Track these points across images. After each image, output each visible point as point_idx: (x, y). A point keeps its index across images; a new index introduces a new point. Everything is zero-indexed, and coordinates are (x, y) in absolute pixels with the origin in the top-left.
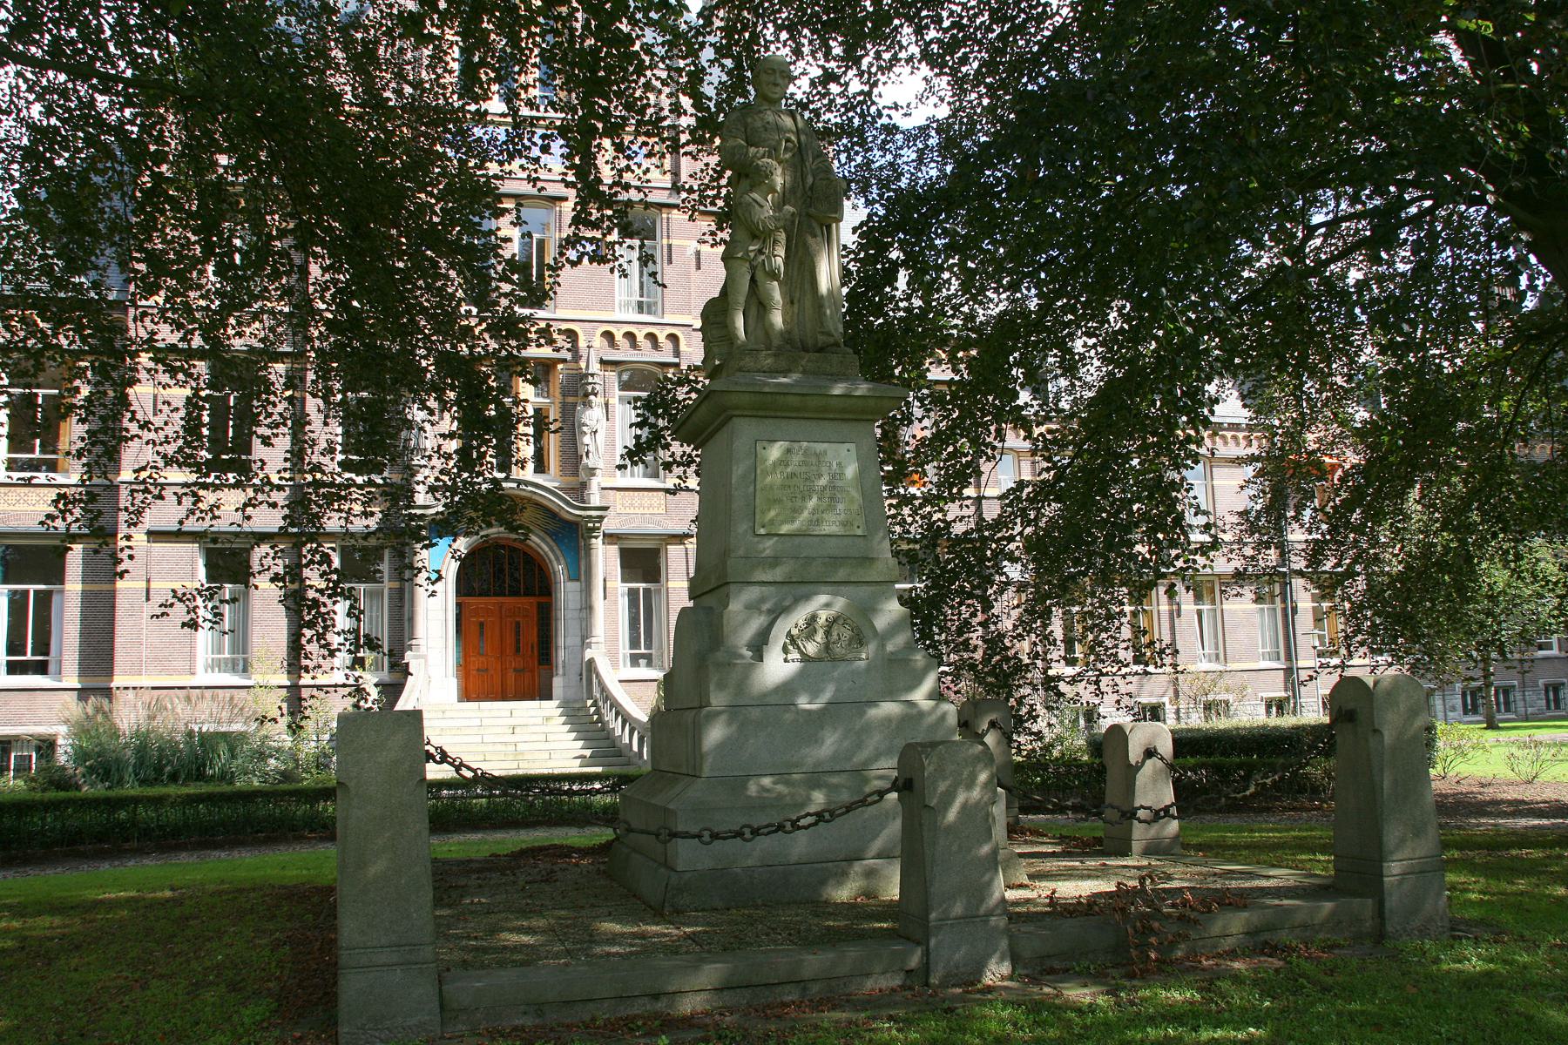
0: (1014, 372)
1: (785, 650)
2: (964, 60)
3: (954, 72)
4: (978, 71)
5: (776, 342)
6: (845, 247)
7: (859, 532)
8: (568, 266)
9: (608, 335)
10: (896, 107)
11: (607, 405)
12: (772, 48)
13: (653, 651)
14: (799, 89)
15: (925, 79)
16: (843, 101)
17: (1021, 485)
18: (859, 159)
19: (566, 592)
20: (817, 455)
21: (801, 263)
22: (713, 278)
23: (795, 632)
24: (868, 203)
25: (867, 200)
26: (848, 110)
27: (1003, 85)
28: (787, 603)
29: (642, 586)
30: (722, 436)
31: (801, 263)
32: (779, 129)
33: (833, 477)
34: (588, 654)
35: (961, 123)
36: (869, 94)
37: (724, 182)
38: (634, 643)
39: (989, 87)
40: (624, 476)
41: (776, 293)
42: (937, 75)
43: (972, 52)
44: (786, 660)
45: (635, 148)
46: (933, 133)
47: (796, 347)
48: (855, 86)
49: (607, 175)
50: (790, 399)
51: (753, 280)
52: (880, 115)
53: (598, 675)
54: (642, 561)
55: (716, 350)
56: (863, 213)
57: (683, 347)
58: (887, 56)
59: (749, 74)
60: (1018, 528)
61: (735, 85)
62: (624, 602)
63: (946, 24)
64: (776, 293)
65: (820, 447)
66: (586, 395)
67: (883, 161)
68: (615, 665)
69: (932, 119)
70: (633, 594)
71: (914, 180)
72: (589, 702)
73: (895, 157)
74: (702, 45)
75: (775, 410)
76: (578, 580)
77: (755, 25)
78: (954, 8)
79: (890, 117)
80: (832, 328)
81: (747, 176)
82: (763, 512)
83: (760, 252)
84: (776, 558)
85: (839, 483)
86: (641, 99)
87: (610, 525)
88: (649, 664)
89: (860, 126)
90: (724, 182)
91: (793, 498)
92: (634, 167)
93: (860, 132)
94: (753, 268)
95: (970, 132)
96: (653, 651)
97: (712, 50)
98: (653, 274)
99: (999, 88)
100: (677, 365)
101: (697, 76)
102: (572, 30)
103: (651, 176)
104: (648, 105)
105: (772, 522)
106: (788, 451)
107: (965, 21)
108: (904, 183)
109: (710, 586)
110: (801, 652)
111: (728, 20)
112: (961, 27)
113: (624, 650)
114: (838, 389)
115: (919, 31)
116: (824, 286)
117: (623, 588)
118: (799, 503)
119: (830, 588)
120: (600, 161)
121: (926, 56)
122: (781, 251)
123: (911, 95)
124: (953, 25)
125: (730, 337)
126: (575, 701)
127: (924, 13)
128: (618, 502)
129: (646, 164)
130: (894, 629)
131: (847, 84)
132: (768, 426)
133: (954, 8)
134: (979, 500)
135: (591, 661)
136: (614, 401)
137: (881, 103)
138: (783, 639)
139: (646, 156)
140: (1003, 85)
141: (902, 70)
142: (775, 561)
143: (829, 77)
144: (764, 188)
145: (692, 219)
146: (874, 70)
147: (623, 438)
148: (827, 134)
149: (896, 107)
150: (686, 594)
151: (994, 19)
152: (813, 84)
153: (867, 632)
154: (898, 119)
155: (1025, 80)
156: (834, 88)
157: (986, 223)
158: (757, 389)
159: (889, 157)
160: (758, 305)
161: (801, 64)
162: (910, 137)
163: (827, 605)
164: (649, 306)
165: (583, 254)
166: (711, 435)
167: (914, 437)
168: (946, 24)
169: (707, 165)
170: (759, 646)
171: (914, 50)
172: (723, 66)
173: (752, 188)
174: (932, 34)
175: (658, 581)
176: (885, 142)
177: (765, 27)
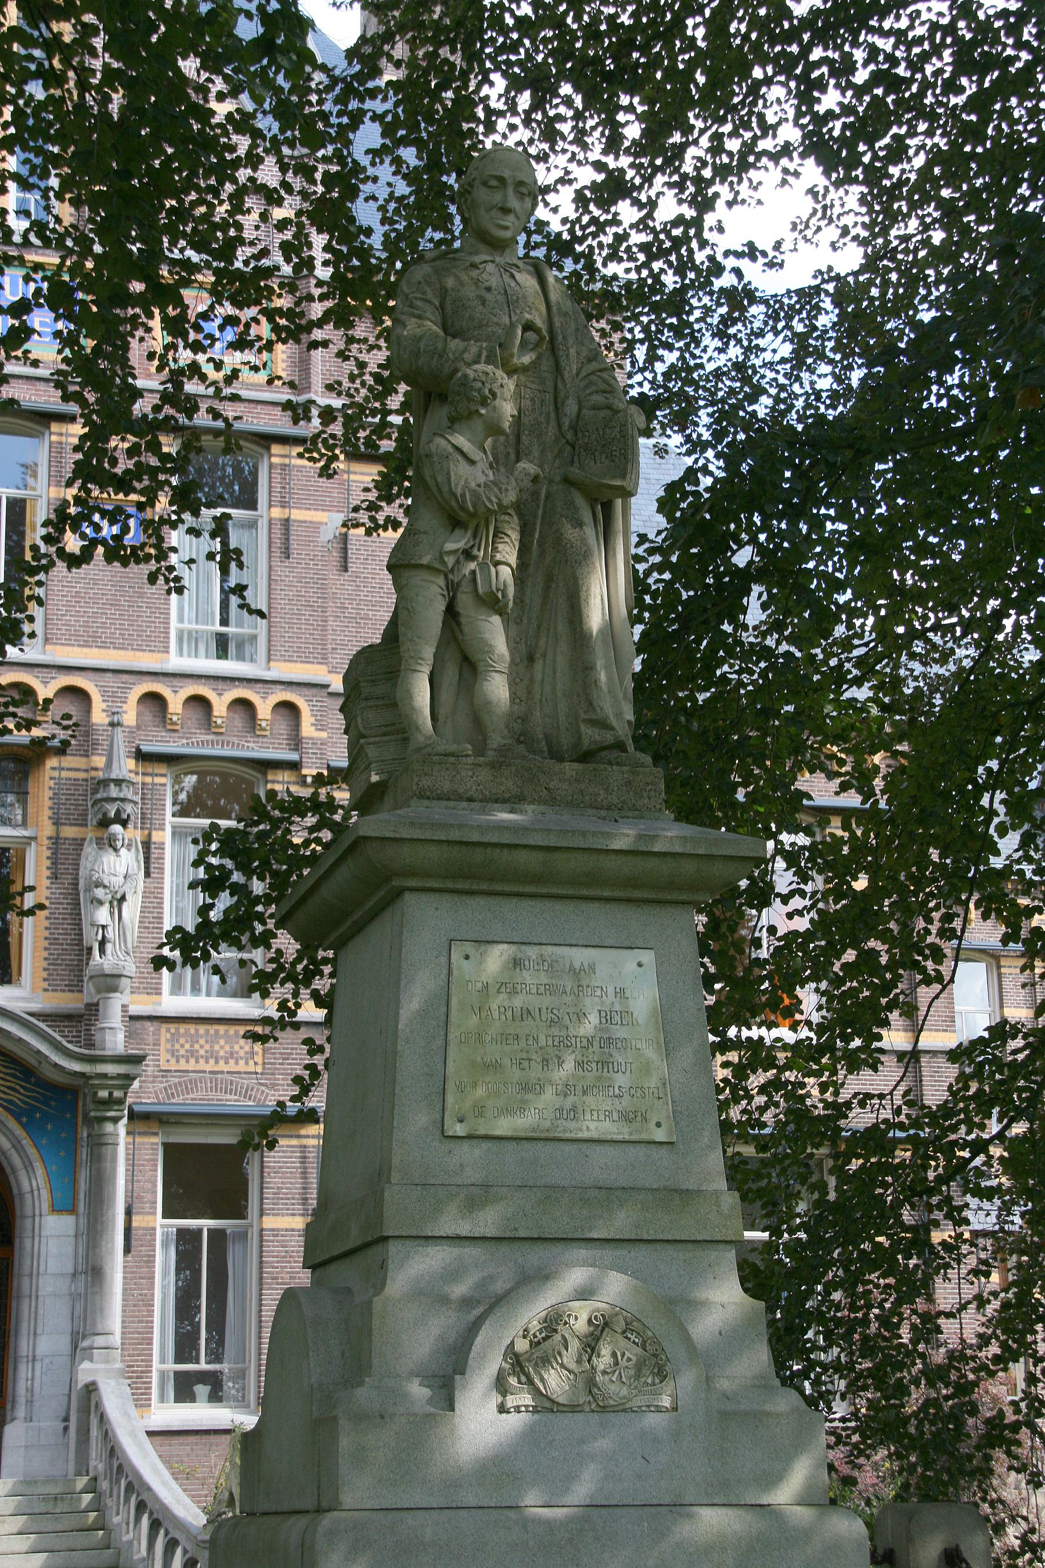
0: (985, 801)
1: (501, 1385)
2: (898, 152)
3: (874, 176)
4: (924, 172)
5: (496, 739)
6: (643, 538)
7: (660, 1135)
8: (61, 566)
9: (154, 700)
10: (752, 252)
11: (147, 845)
12: (502, 124)
13: (225, 1367)
14: (558, 211)
15: (812, 192)
16: (643, 238)
17: (1001, 1031)
18: (671, 357)
19: (49, 1239)
20: (576, 973)
21: (549, 579)
22: (368, 603)
23: (522, 1346)
24: (696, 446)
25: (688, 439)
26: (651, 257)
27: (974, 201)
28: (500, 1286)
29: (206, 1224)
30: (378, 934)
31: (549, 579)
32: (511, 301)
33: (607, 1017)
34: (87, 1371)
35: (886, 284)
36: (697, 223)
37: (394, 402)
38: (185, 1348)
39: (948, 208)
40: (177, 988)
41: (495, 636)
42: (838, 184)
43: (912, 133)
44: (502, 1409)
45: (211, 327)
46: (827, 304)
47: (546, 751)
48: (669, 208)
49: (149, 380)
50: (522, 858)
51: (451, 612)
52: (717, 269)
53: (103, 1418)
54: (209, 1174)
55: (372, 752)
56: (674, 469)
57: (307, 729)
58: (733, 145)
59: (451, 179)
60: (994, 1127)
61: (427, 202)
62: (163, 1261)
63: (861, 77)
64: (495, 636)
65: (580, 956)
66: (105, 823)
67: (722, 360)
68: (141, 1400)
69: (827, 275)
70: (187, 1240)
71: (782, 405)
72: (82, 1482)
73: (748, 350)
74: (356, 119)
75: (482, 875)
76: (72, 1210)
77: (465, 76)
78: (880, 43)
79: (738, 272)
80: (609, 712)
81: (443, 398)
82: (461, 1089)
83: (469, 554)
84: (486, 1186)
85: (620, 1032)
86: (224, 226)
87: (144, 1093)
88: (216, 1397)
89: (677, 290)
90: (394, 402)
91: (523, 1062)
92: (208, 369)
93: (677, 302)
94: (452, 589)
95: (903, 305)
96: (225, 1367)
97: (376, 128)
98: (240, 590)
99: (967, 210)
100: (294, 766)
101: (348, 180)
102: (84, 73)
103: (254, 380)
104: (240, 241)
105: (479, 1110)
106: (517, 963)
107: (901, 71)
108: (762, 408)
109: (347, 1242)
110: (536, 1393)
111: (412, 64)
112: (895, 84)
113: (162, 1362)
114: (624, 837)
115: (807, 91)
116: (595, 618)
117: (161, 1227)
118: (535, 1072)
119: (595, 1252)
120: (136, 352)
121: (817, 146)
122: (509, 552)
123: (785, 226)
124: (877, 78)
125: (400, 728)
126: (50, 1480)
127: (817, 54)
128: (164, 1053)
129: (234, 359)
130: (732, 1340)
131: (652, 204)
132: (475, 912)
133: (880, 43)
134: (911, 1058)
135: (91, 1388)
136: (164, 836)
137: (723, 243)
138: (495, 1363)
139: (234, 346)
140: (974, 201)
141: (767, 175)
142: (480, 1195)
143: (613, 189)
144: (478, 425)
145: (326, 472)
146: (707, 173)
147: (179, 911)
148: (615, 302)
149: (752, 252)
150: (297, 1246)
151: (964, 64)
152: (580, 200)
153: (674, 1349)
154: (754, 273)
155: (1024, 190)
156: (627, 212)
157: (935, 492)
158: (455, 835)
159: (735, 352)
160: (462, 660)
161: (560, 160)
162: (779, 312)
163: (584, 1294)
164: (240, 646)
165: (94, 543)
166: (359, 928)
167: (772, 930)
168: (861, 77)
169: (362, 365)
170: (446, 1380)
171: (790, 134)
172: (398, 161)
173: (454, 421)
174: (830, 100)
175: (239, 1212)
176: (727, 321)
177: (486, 80)
